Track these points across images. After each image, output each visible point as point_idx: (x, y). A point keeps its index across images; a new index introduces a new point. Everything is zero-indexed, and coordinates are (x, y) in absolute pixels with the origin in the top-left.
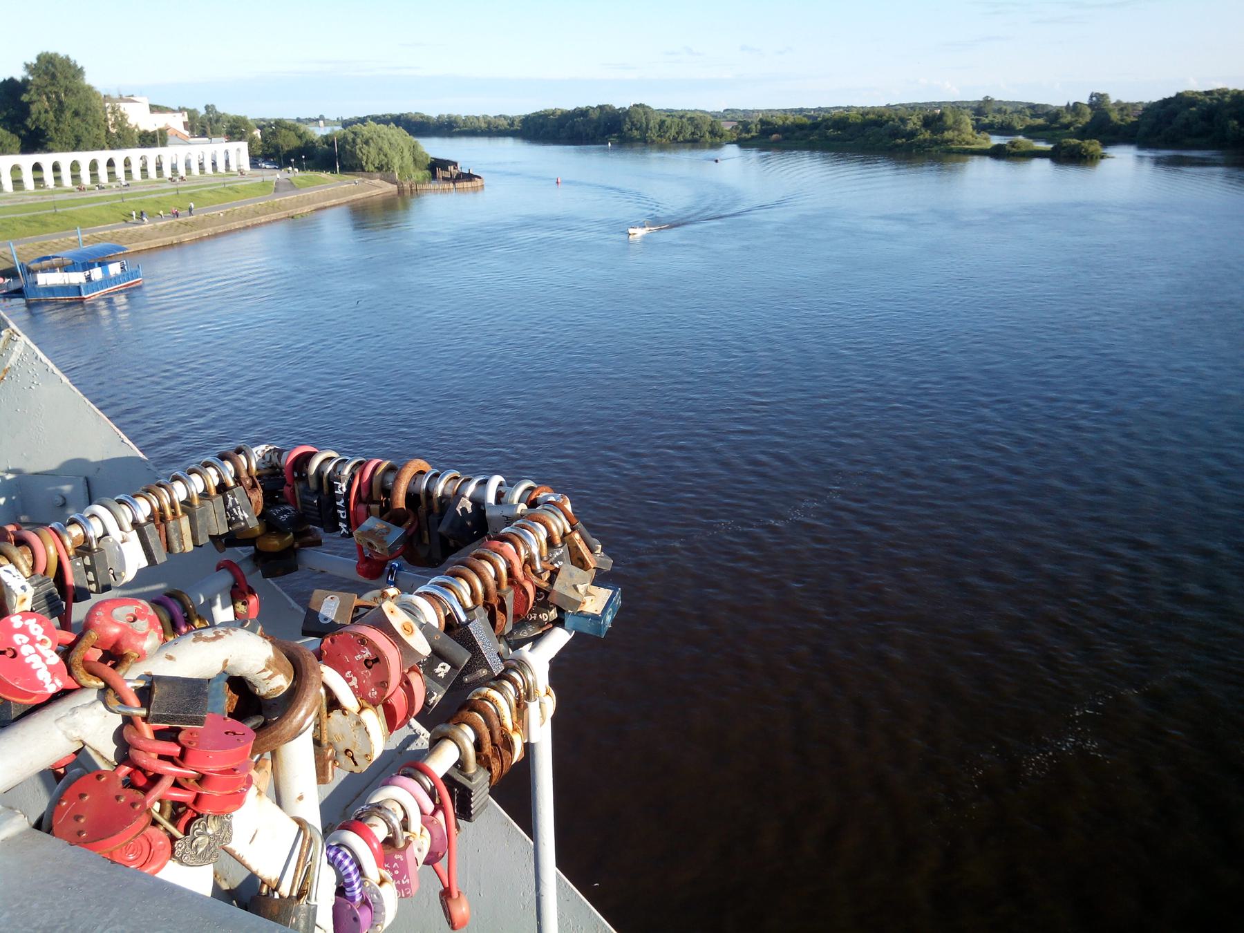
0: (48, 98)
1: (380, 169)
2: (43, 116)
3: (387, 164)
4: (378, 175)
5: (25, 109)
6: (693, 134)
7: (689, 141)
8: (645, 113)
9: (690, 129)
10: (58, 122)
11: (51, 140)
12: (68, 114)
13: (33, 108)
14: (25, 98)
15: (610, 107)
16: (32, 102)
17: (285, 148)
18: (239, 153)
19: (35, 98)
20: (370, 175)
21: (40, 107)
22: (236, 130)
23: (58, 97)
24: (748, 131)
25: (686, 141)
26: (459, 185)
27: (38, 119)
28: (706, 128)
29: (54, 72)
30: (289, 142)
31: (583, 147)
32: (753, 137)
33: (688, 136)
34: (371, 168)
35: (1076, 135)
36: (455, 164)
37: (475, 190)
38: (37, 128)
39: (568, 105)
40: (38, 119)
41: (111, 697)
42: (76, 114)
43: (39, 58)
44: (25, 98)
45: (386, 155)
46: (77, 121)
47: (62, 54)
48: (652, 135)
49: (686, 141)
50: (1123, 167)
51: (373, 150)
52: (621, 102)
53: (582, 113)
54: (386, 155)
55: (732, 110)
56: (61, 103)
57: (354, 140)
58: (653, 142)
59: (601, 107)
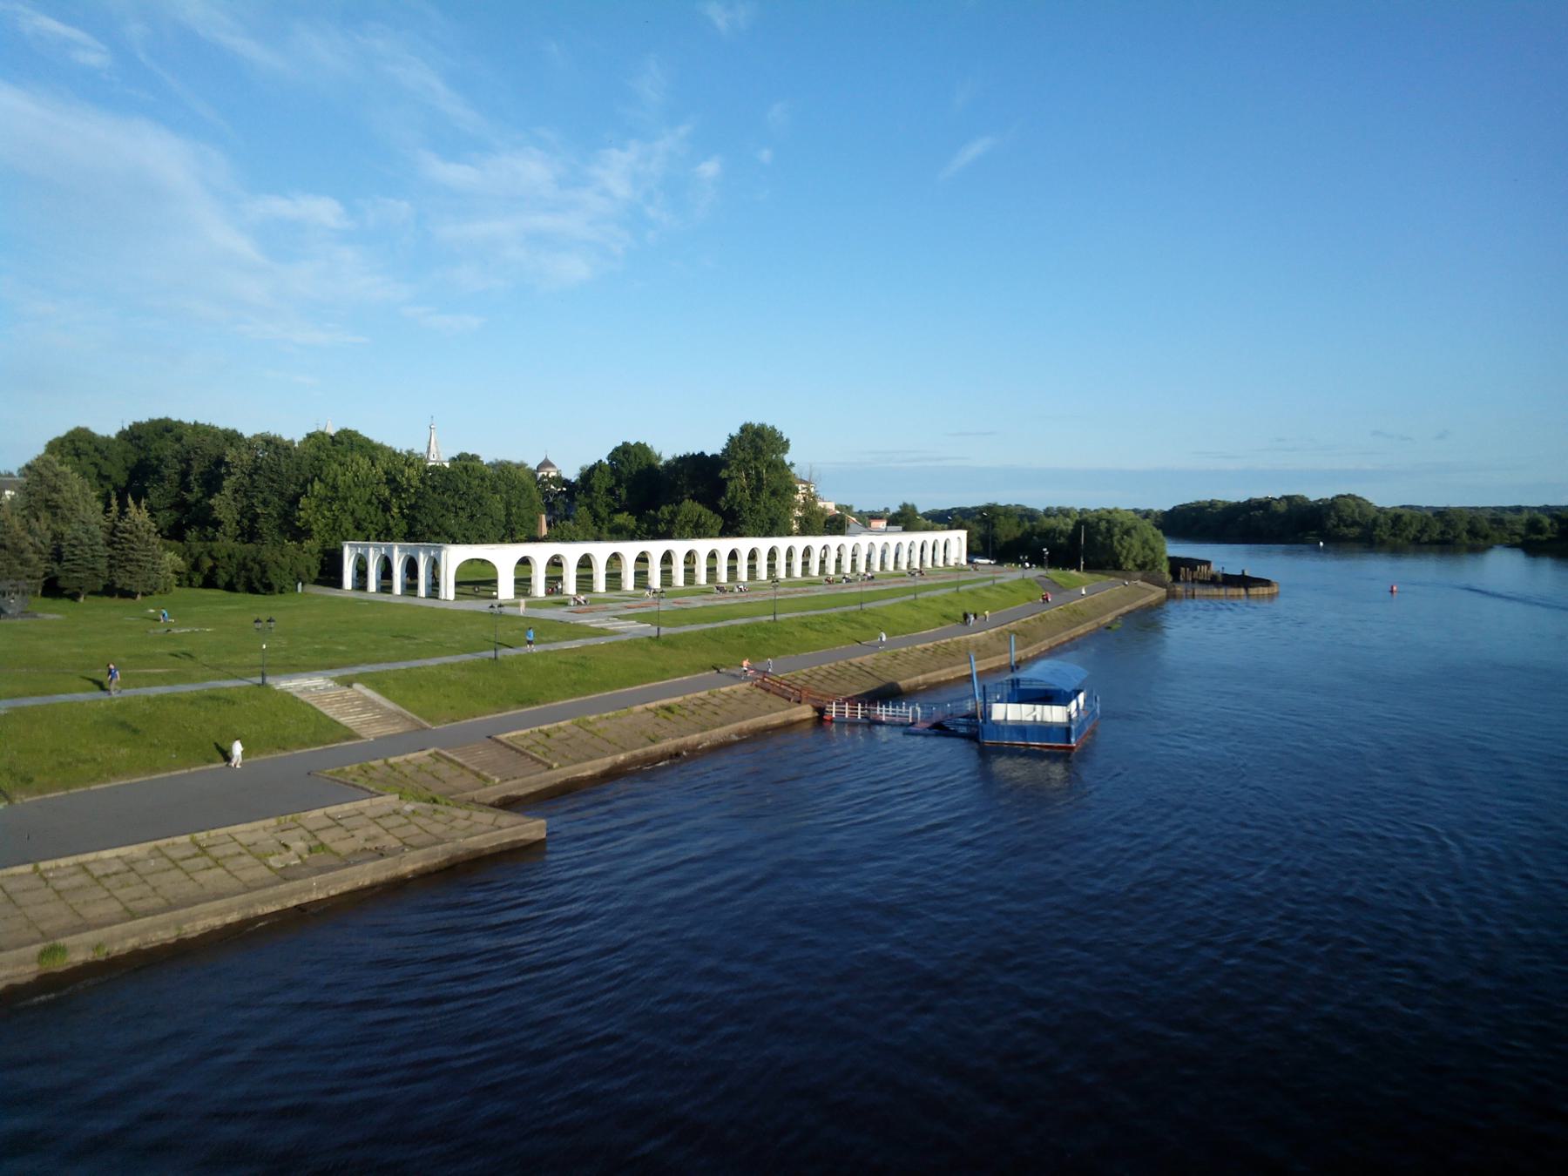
0: (747, 475)
1: (1141, 567)
2: (739, 494)
3: (1153, 561)
4: (1139, 574)
5: (721, 486)
6: (1443, 533)
7: (1437, 542)
8: (1359, 505)
9: (1438, 527)
10: (754, 501)
11: (744, 522)
12: (765, 495)
13: (731, 485)
14: (724, 474)
15: (1302, 498)
16: (731, 478)
17: (1003, 536)
18: (956, 542)
19: (734, 474)
20: (1127, 574)
21: (738, 483)
22: (943, 519)
23: (758, 473)
24: (1541, 531)
25: (1432, 542)
26: (1253, 591)
27: (734, 497)
28: (1463, 526)
29: (758, 447)
30: (1007, 531)
31: (1253, 547)
32: (1550, 540)
33: (1436, 536)
34: (1130, 565)
35: (1448, 534)
36: (1208, 563)
37: (1272, 596)
38: (730, 508)
39: (1237, 494)
40: (734, 497)
41: (330, 822)
42: (774, 493)
43: (743, 430)
44: (724, 474)
45: (1152, 550)
46: (773, 501)
47: (769, 424)
48: (1383, 533)
49: (1432, 542)
50: (1504, 567)
51: (1137, 544)
52: (1316, 493)
53: (1264, 505)
54: (1152, 550)
55: (1411, 507)
56: (760, 480)
57: (1109, 530)
58: (1383, 542)
59: (1288, 499)
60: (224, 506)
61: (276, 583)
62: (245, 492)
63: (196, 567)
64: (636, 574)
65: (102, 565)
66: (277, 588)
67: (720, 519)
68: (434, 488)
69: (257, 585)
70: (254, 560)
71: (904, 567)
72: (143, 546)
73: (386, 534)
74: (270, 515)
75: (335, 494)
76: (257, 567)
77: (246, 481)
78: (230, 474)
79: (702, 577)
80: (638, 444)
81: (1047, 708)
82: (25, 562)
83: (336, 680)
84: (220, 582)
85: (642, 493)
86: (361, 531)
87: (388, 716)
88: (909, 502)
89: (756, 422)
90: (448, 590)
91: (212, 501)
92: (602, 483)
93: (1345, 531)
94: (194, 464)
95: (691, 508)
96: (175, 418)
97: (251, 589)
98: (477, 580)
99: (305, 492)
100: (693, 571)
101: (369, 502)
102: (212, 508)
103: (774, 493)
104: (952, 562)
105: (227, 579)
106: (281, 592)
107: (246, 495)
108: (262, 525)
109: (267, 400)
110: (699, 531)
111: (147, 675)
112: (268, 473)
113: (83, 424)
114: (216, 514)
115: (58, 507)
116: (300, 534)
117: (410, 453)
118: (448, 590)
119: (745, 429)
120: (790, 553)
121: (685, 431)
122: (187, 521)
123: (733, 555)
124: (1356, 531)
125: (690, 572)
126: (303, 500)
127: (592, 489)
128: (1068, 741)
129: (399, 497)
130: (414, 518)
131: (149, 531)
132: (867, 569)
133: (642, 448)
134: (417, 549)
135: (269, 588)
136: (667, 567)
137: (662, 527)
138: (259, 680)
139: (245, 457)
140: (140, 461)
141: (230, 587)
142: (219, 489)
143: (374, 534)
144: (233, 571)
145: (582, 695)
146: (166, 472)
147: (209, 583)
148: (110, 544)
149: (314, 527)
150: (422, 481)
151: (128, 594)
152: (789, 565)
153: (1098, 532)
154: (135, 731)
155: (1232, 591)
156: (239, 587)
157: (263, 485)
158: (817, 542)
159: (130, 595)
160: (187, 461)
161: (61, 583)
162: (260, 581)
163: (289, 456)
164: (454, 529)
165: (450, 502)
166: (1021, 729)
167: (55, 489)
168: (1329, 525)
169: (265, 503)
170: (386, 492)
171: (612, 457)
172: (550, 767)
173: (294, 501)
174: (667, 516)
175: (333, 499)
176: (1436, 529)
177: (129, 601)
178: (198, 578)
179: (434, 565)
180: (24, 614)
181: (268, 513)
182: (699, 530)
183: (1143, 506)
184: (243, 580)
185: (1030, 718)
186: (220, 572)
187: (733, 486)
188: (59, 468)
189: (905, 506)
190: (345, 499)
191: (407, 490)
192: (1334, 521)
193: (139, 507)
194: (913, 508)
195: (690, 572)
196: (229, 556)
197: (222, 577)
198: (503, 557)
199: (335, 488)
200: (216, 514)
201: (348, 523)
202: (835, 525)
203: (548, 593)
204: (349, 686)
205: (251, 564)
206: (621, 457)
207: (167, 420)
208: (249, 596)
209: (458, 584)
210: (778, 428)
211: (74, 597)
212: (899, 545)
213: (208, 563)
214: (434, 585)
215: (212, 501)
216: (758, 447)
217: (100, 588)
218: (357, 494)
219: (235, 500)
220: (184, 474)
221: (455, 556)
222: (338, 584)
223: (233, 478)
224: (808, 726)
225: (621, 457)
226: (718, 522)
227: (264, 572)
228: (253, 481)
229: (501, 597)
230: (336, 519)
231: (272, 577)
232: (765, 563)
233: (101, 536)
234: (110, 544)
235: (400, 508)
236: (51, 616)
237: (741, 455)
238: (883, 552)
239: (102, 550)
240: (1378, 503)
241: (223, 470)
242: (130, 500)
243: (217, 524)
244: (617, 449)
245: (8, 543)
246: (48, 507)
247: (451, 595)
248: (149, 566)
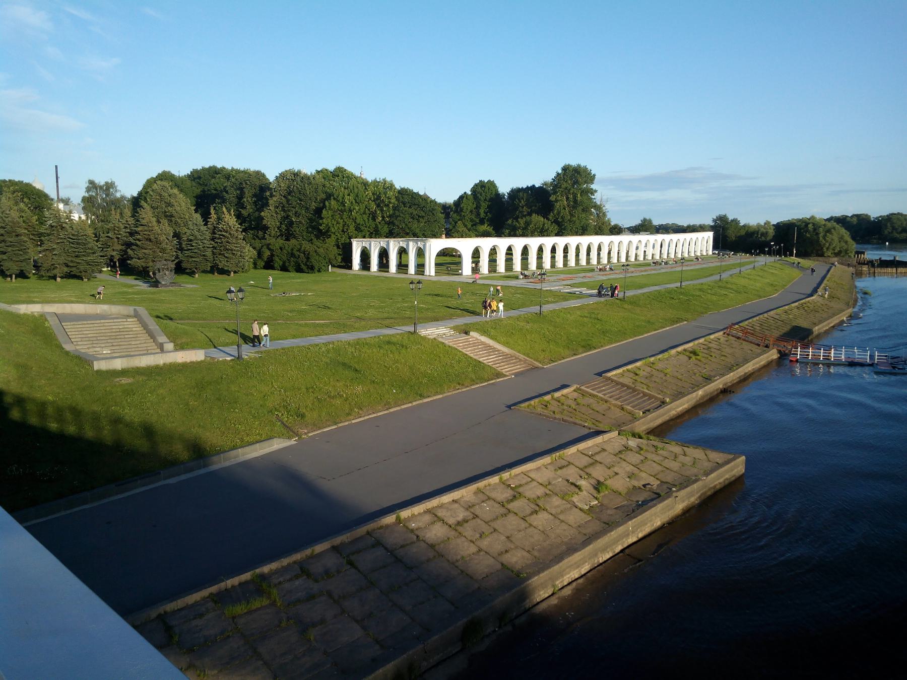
0: (567, 198)
2: (563, 211)
10: (572, 215)
13: (557, 205)
16: (557, 201)
17: (731, 238)
21: (561, 203)
29: (575, 179)
40: (559, 213)
42: (583, 210)
47: (583, 165)
51: (835, 238)
56: (575, 201)
57: (815, 230)
59: (857, 216)
63: (260, 255)
64: (506, 260)
65: (209, 253)
68: (404, 204)
70: (299, 250)
71: (632, 259)
73: (375, 234)
74: (300, 222)
75: (343, 210)
78: (272, 196)
79: (501, 267)
80: (489, 181)
82: (163, 250)
83: (455, 328)
85: (494, 211)
87: (507, 358)
89: (573, 163)
90: (430, 269)
91: (262, 214)
92: (468, 206)
95: (537, 219)
96: (219, 166)
97: (299, 270)
98: (449, 259)
99: (324, 206)
100: (495, 261)
103: (583, 210)
106: (319, 271)
107: (284, 210)
108: (296, 229)
109: (273, 151)
110: (543, 233)
112: (298, 195)
113: (167, 169)
114: (265, 222)
115: (172, 216)
116: (322, 234)
117: (384, 180)
118: (430, 269)
119: (565, 169)
120: (553, 250)
121: (520, 170)
123: (540, 250)
125: (493, 261)
127: (462, 210)
132: (627, 259)
133: (491, 184)
135: (311, 269)
140: (204, 191)
141: (284, 269)
142: (267, 205)
144: (285, 258)
145: (616, 342)
146: (227, 196)
147: (269, 266)
148: (213, 239)
150: (397, 198)
151: (223, 272)
153: (807, 231)
156: (290, 268)
158: (605, 240)
160: (241, 189)
161: (184, 265)
162: (306, 265)
164: (417, 231)
165: (415, 213)
167: (169, 204)
168: (886, 232)
169: (297, 214)
171: (474, 190)
172: (162, 350)
173: (318, 211)
174: (522, 225)
175: (342, 211)
177: (225, 277)
178: (261, 263)
179: (420, 253)
180: (173, 284)
181: (301, 221)
182: (543, 232)
183: (838, 213)
184: (292, 263)
186: (276, 259)
187: (560, 204)
188: (171, 191)
189: (645, 220)
190: (350, 211)
191: (388, 205)
192: (889, 229)
194: (650, 221)
196: (281, 248)
197: (278, 262)
198: (464, 246)
202: (616, 230)
203: (490, 272)
204: (466, 333)
205: (297, 253)
206: (479, 190)
207: (214, 167)
209: (436, 264)
210: (589, 168)
211: (192, 274)
213: (267, 253)
214: (420, 267)
216: (575, 179)
217: (209, 269)
218: (357, 208)
220: (240, 197)
221: (435, 245)
222: (350, 267)
224: (774, 364)
225: (479, 190)
226: (556, 228)
227: (308, 258)
228: (288, 201)
231: (314, 261)
232: (562, 255)
233: (208, 235)
234: (213, 239)
235: (383, 217)
236: (189, 286)
237: (564, 185)
239: (207, 243)
241: (268, 194)
243: (265, 228)
244: (476, 185)
245: (152, 237)
246: (166, 216)
247: (433, 273)
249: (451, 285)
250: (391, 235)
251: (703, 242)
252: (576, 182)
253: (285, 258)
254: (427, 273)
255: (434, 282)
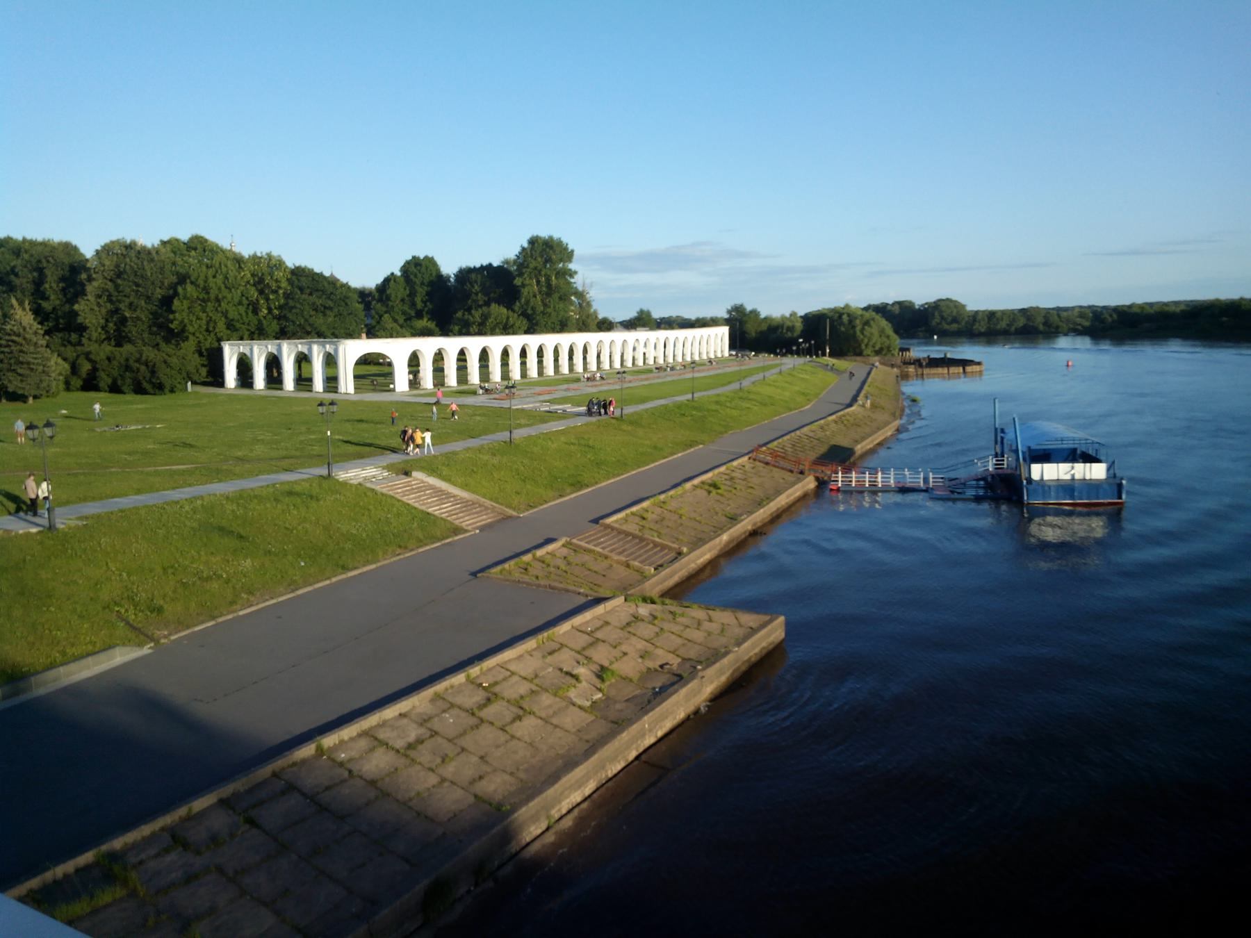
0: (538, 282)
2: (532, 300)
8: (956, 307)
10: (545, 305)
13: (525, 291)
16: (523, 285)
17: (749, 334)
19: (527, 282)
21: (530, 288)
26: (969, 369)
28: (1040, 320)
29: (545, 256)
35: (1030, 328)
40: (528, 302)
56: (549, 286)
57: (850, 321)
59: (900, 303)
60: (89, 311)
61: (167, 383)
62: (110, 296)
63: (74, 369)
66: (168, 387)
67: (525, 321)
68: (301, 289)
69: (146, 385)
70: (138, 361)
72: (32, 349)
73: (258, 333)
74: (138, 318)
75: (206, 297)
76: (143, 368)
77: (110, 285)
78: (90, 279)
80: (426, 257)
81: (1047, 466)
83: (389, 468)
84: (102, 384)
85: (436, 299)
86: (236, 331)
88: (645, 309)
89: (544, 233)
90: (347, 384)
91: (76, 307)
93: (946, 327)
94: (47, 272)
97: (139, 390)
98: (374, 371)
100: (442, 370)
101: (240, 303)
102: (76, 314)
103: (560, 298)
104: (688, 359)
105: (110, 381)
106: (172, 391)
108: (132, 330)
110: (507, 329)
111: (172, 474)
114: (80, 320)
116: (175, 336)
117: (269, 255)
118: (347, 384)
119: (533, 241)
120: (523, 353)
121: (470, 243)
122: (62, 326)
124: (276, 374)
125: (439, 370)
126: (176, 302)
127: (388, 298)
128: (1120, 498)
129: (267, 299)
130: (285, 318)
131: (36, 333)
134: (310, 345)
135: (159, 388)
136: (331, 373)
137: (475, 328)
138: (324, 472)
139: (107, 263)
141: (115, 389)
143: (247, 333)
144: (115, 373)
145: (619, 475)
146: (17, 281)
149: (191, 329)
152: (523, 364)
153: (842, 324)
154: (241, 537)
155: (940, 370)
156: (124, 388)
157: (128, 290)
159: (22, 398)
160: (40, 270)
162: (150, 382)
163: (152, 260)
164: (323, 329)
166: (1068, 487)
168: (934, 323)
170: (254, 294)
173: (167, 302)
175: (204, 300)
176: (1021, 322)
177: (19, 405)
182: (507, 329)
183: (876, 300)
184: (128, 381)
185: (1068, 477)
186: (102, 375)
187: (528, 289)
189: (642, 312)
191: (275, 292)
193: (24, 309)
195: (439, 370)
196: (109, 359)
197: (104, 380)
198: (397, 349)
199: (206, 290)
200: (80, 320)
201: (221, 325)
204: (407, 474)
206: (413, 269)
208: (139, 397)
209: (356, 377)
210: (565, 240)
212: (462, 352)
213: (86, 367)
214: (332, 381)
215: (76, 307)
216: (545, 256)
218: (229, 296)
219: (99, 305)
221: (352, 350)
222: (221, 383)
223: (95, 284)
226: (524, 323)
227: (153, 372)
228: (117, 287)
229: (397, 390)
230: (210, 320)
231: (163, 375)
238: (585, 351)
240: (971, 307)
241: (84, 276)
242: (14, 301)
243: (82, 329)
244: (408, 263)
247: (351, 390)
248: (41, 368)
249: (378, 406)
250: (283, 334)
251: (716, 341)
252: (548, 260)
253: (115, 373)
254: (342, 389)
255: (354, 403)
